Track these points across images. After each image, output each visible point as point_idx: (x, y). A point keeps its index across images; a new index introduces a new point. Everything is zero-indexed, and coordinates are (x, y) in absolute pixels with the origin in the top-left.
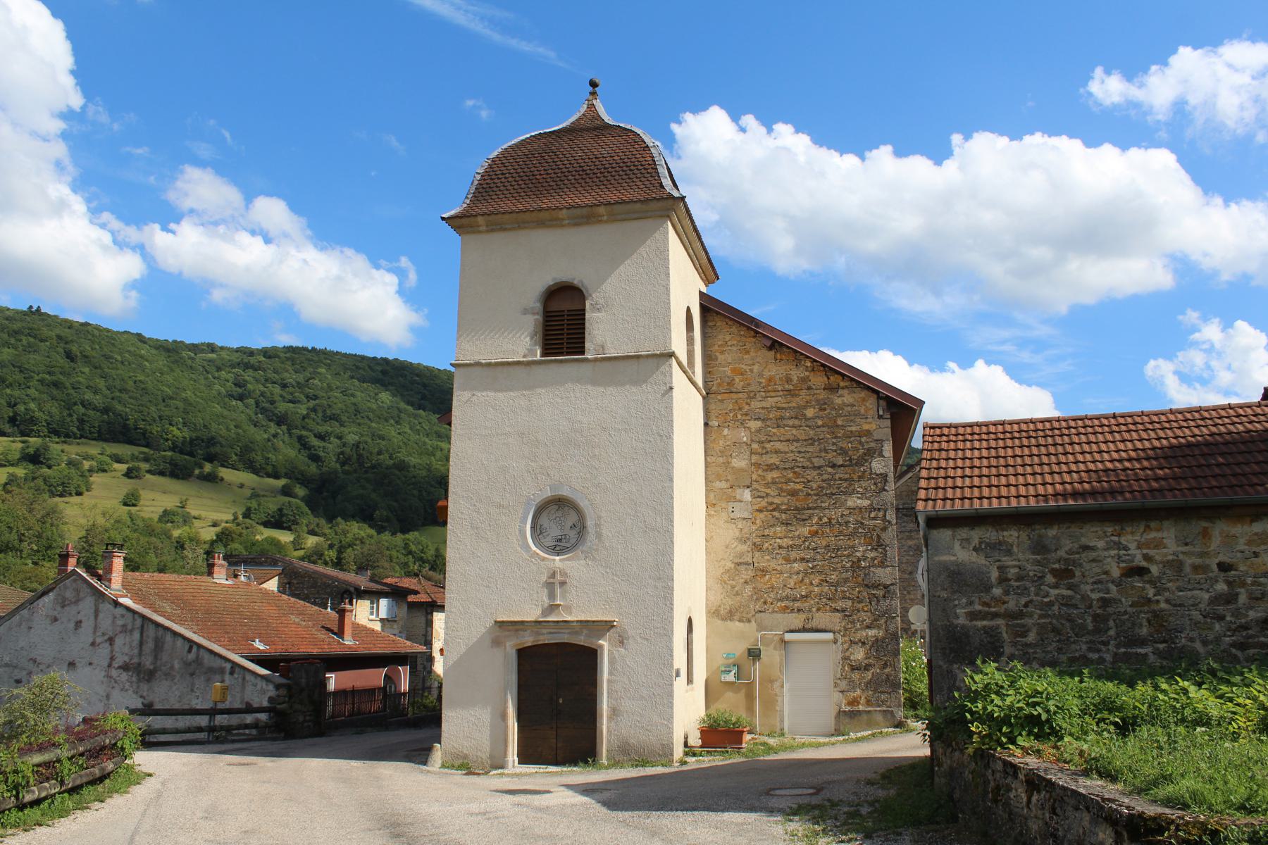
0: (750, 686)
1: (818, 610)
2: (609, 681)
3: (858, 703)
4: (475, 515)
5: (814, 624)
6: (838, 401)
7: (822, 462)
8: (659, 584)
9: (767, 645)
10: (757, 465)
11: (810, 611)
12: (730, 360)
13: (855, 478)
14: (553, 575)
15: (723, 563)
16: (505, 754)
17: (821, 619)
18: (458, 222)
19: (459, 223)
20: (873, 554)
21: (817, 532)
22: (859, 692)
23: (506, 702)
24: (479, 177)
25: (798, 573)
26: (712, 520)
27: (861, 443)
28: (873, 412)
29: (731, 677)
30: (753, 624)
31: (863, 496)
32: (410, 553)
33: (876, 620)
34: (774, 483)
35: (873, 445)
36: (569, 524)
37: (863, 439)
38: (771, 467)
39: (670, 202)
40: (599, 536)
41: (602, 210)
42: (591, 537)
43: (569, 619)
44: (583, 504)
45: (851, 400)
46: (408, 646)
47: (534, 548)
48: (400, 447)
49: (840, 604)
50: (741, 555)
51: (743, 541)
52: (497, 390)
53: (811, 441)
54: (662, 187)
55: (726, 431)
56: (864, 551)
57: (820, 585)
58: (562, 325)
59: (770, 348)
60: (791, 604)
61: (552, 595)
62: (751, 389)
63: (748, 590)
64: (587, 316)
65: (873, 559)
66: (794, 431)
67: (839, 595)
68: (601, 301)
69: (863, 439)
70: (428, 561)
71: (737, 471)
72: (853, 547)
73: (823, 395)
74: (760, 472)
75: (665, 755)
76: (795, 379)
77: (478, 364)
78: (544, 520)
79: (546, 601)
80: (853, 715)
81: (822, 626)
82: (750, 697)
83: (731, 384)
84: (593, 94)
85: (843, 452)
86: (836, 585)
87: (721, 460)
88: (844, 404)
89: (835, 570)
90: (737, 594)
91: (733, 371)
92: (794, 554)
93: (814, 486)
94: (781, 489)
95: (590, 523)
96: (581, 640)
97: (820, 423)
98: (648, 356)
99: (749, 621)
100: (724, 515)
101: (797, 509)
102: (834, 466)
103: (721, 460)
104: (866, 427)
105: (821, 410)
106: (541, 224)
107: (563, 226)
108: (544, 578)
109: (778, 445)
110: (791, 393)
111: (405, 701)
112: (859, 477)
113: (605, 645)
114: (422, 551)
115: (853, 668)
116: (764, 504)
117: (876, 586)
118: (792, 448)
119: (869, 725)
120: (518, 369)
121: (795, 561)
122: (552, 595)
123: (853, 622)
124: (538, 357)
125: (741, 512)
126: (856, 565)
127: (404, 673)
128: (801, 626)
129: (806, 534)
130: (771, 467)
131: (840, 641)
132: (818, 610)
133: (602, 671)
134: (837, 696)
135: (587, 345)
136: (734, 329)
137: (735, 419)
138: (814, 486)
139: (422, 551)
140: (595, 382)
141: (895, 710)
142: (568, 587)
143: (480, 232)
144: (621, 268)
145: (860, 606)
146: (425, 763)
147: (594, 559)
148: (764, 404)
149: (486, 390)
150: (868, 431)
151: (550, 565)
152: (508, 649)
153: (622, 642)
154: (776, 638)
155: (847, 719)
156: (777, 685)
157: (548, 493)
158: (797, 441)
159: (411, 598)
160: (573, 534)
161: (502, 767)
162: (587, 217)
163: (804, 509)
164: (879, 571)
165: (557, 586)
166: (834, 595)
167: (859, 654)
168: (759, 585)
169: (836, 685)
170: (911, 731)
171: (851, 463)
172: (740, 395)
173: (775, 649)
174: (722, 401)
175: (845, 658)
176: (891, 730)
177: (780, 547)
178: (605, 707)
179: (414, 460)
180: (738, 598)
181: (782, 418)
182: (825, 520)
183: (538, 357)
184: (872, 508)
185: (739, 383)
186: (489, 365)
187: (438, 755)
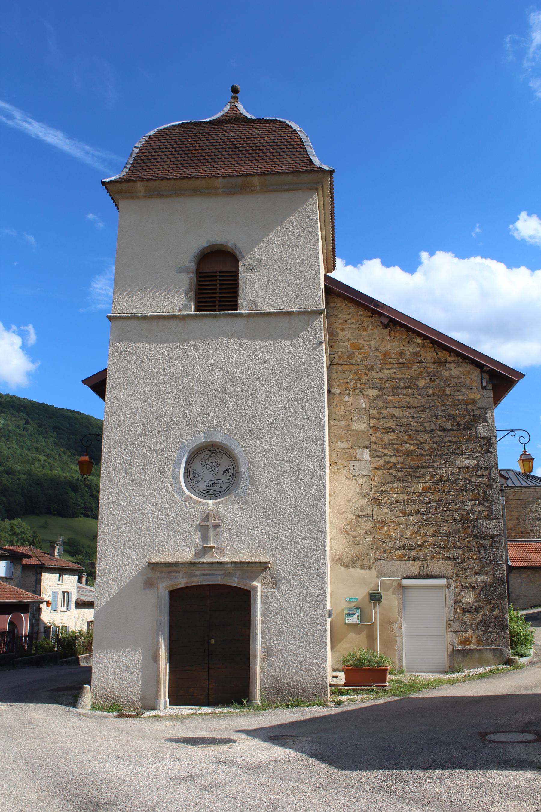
0: (371, 628)
1: (432, 558)
2: (262, 622)
3: (470, 643)
4: (128, 459)
5: (429, 570)
6: (446, 374)
7: (433, 427)
8: (312, 527)
9: (386, 590)
10: (375, 429)
11: (425, 559)
12: (349, 336)
13: (463, 440)
14: (207, 518)
15: (345, 515)
16: (157, 696)
17: (435, 566)
18: (118, 187)
19: (117, 190)
20: (480, 508)
21: (430, 488)
22: (470, 632)
23: (158, 643)
24: (137, 150)
25: (413, 525)
26: (335, 477)
27: (467, 410)
28: (476, 384)
29: (354, 619)
30: (374, 571)
31: (470, 457)
32: (15, 534)
33: (484, 567)
34: (391, 444)
35: (478, 412)
36: (222, 469)
37: (469, 407)
38: (387, 431)
39: (320, 175)
40: (252, 480)
41: (256, 180)
42: (244, 481)
43: (223, 560)
44: (237, 450)
45: (458, 373)
46: (27, 596)
47: (187, 492)
48: (8, 457)
49: (452, 553)
50: (362, 508)
51: (363, 495)
52: (151, 342)
53: (423, 408)
54: (311, 162)
55: (347, 398)
56: (473, 505)
57: (433, 535)
58: (216, 284)
59: (385, 326)
60: (408, 551)
61: (205, 538)
62: (368, 361)
63: (369, 540)
64: (240, 276)
65: (481, 512)
66: (408, 399)
67: (451, 544)
68: (254, 263)
69: (469, 407)
70: (28, 540)
71: (357, 434)
72: (462, 502)
73: (433, 368)
74: (378, 434)
75: (319, 695)
76: (408, 353)
77: (134, 317)
78: (197, 466)
80: (466, 653)
81: (436, 573)
82: (371, 638)
83: (351, 356)
84: (235, 98)
85: (452, 418)
86: (448, 535)
87: (343, 423)
88: (451, 376)
89: (446, 522)
90: (358, 543)
91: (353, 345)
92: (409, 508)
93: (427, 447)
94: (397, 450)
95: (243, 468)
96: (235, 582)
97: (431, 392)
98: (299, 313)
99: (370, 568)
100: (346, 472)
101: (411, 467)
102: (444, 430)
103: (343, 423)
104: (471, 396)
105: (431, 381)
106: (197, 192)
107: (217, 195)
108: (198, 521)
109: (394, 411)
110: (404, 366)
111: (25, 643)
112: (467, 440)
114: (24, 533)
115: (465, 611)
116: (382, 462)
117: (483, 537)
118: (406, 414)
119: (481, 663)
120: (174, 323)
121: (411, 514)
122: (205, 538)
123: (464, 569)
124: (193, 312)
125: (361, 470)
126: (465, 519)
127: (26, 619)
128: (417, 573)
129: (420, 489)
130: (387, 431)
131: (453, 585)
132: (432, 558)
134: (451, 636)
135: (240, 302)
136: (353, 309)
137: (355, 388)
138: (427, 447)
139: (24, 533)
140: (248, 336)
141: (503, 648)
142: (221, 529)
143: (138, 198)
144: (273, 233)
145: (470, 554)
146: (74, 706)
147: (247, 503)
148: (380, 375)
149: (141, 341)
150: (473, 400)
151: (204, 508)
152: (161, 590)
153: (275, 584)
154: (395, 584)
155: (460, 658)
156: (396, 626)
157: (201, 439)
158: (411, 407)
159: (25, 561)
160: (225, 479)
161: (154, 709)
162: (240, 187)
163: (418, 467)
164: (486, 523)
165: (211, 529)
166: (446, 544)
167: (470, 598)
168: (379, 536)
169: (449, 626)
170: (522, 668)
171: (459, 428)
172: (359, 367)
173: (394, 593)
174: (343, 371)
175: (457, 602)
176: (501, 667)
177: (397, 501)
178: (259, 647)
179: (18, 467)
180: (360, 547)
181: (397, 387)
182: (437, 477)
183: (193, 312)
184: (478, 467)
185: (358, 357)
186: (145, 318)
187: (88, 697)
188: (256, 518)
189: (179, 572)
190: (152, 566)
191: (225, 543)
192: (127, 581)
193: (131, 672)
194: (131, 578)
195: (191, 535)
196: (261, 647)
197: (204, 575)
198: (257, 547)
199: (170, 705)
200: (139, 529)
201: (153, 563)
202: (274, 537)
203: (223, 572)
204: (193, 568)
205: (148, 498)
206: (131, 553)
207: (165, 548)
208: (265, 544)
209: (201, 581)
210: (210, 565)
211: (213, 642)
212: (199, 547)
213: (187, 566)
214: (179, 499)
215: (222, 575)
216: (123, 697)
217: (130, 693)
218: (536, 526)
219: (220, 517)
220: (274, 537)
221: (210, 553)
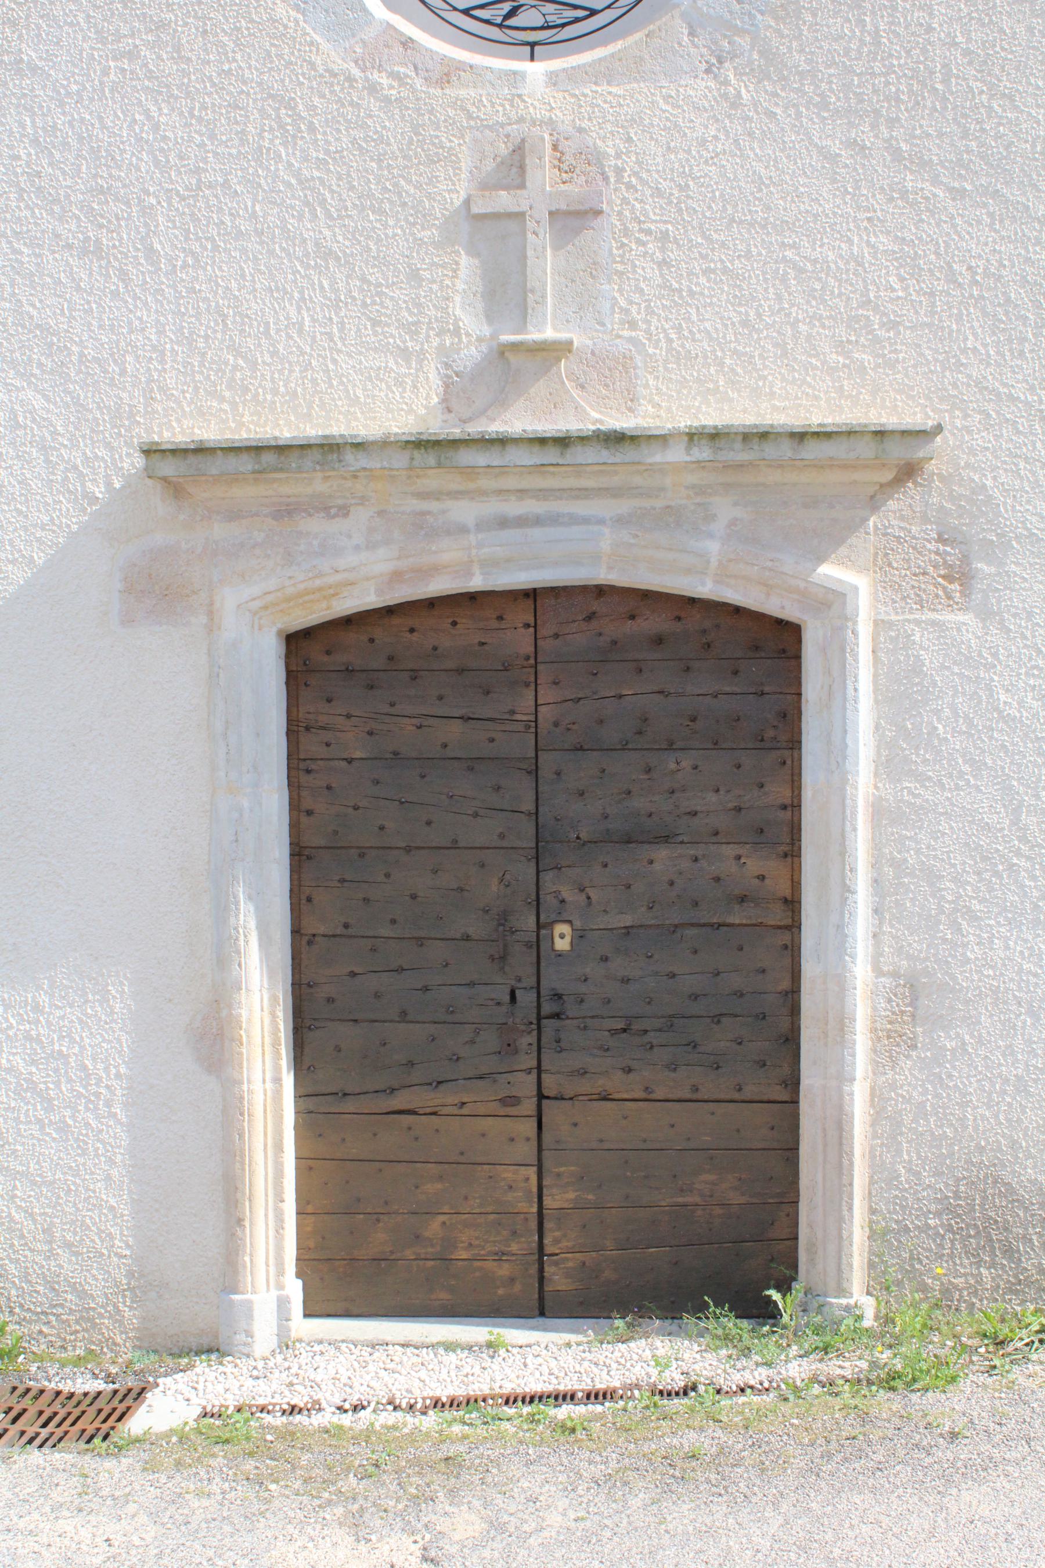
2: (878, 812)
14: (515, 166)
16: (229, 1274)
23: (223, 955)
79: (473, 330)
96: (705, 566)
108: (455, 190)
113: (858, 604)
122: (506, 290)
133: (839, 756)
152: (233, 623)
153: (960, 575)
161: (212, 1348)
178: (861, 971)
188: (833, 159)
189: (344, 511)
190: (168, 468)
191: (633, 325)
192: (19, 575)
193: (63, 1128)
194: (40, 558)
195: (414, 275)
196: (878, 971)
197: (503, 523)
198: (841, 347)
199: (309, 1313)
200: (84, 252)
201: (178, 452)
202: (952, 278)
203: (624, 506)
204: (433, 481)
205: (132, 55)
206: (38, 402)
207: (254, 365)
208: (894, 325)
209: (490, 564)
210: (551, 455)
211: (562, 938)
212: (470, 354)
213: (400, 460)
214: (331, 54)
215: (621, 521)
216: (26, 1277)
217: (64, 1255)
218: (1012, 590)
219: (594, 159)
220: (952, 278)
221: (540, 389)
